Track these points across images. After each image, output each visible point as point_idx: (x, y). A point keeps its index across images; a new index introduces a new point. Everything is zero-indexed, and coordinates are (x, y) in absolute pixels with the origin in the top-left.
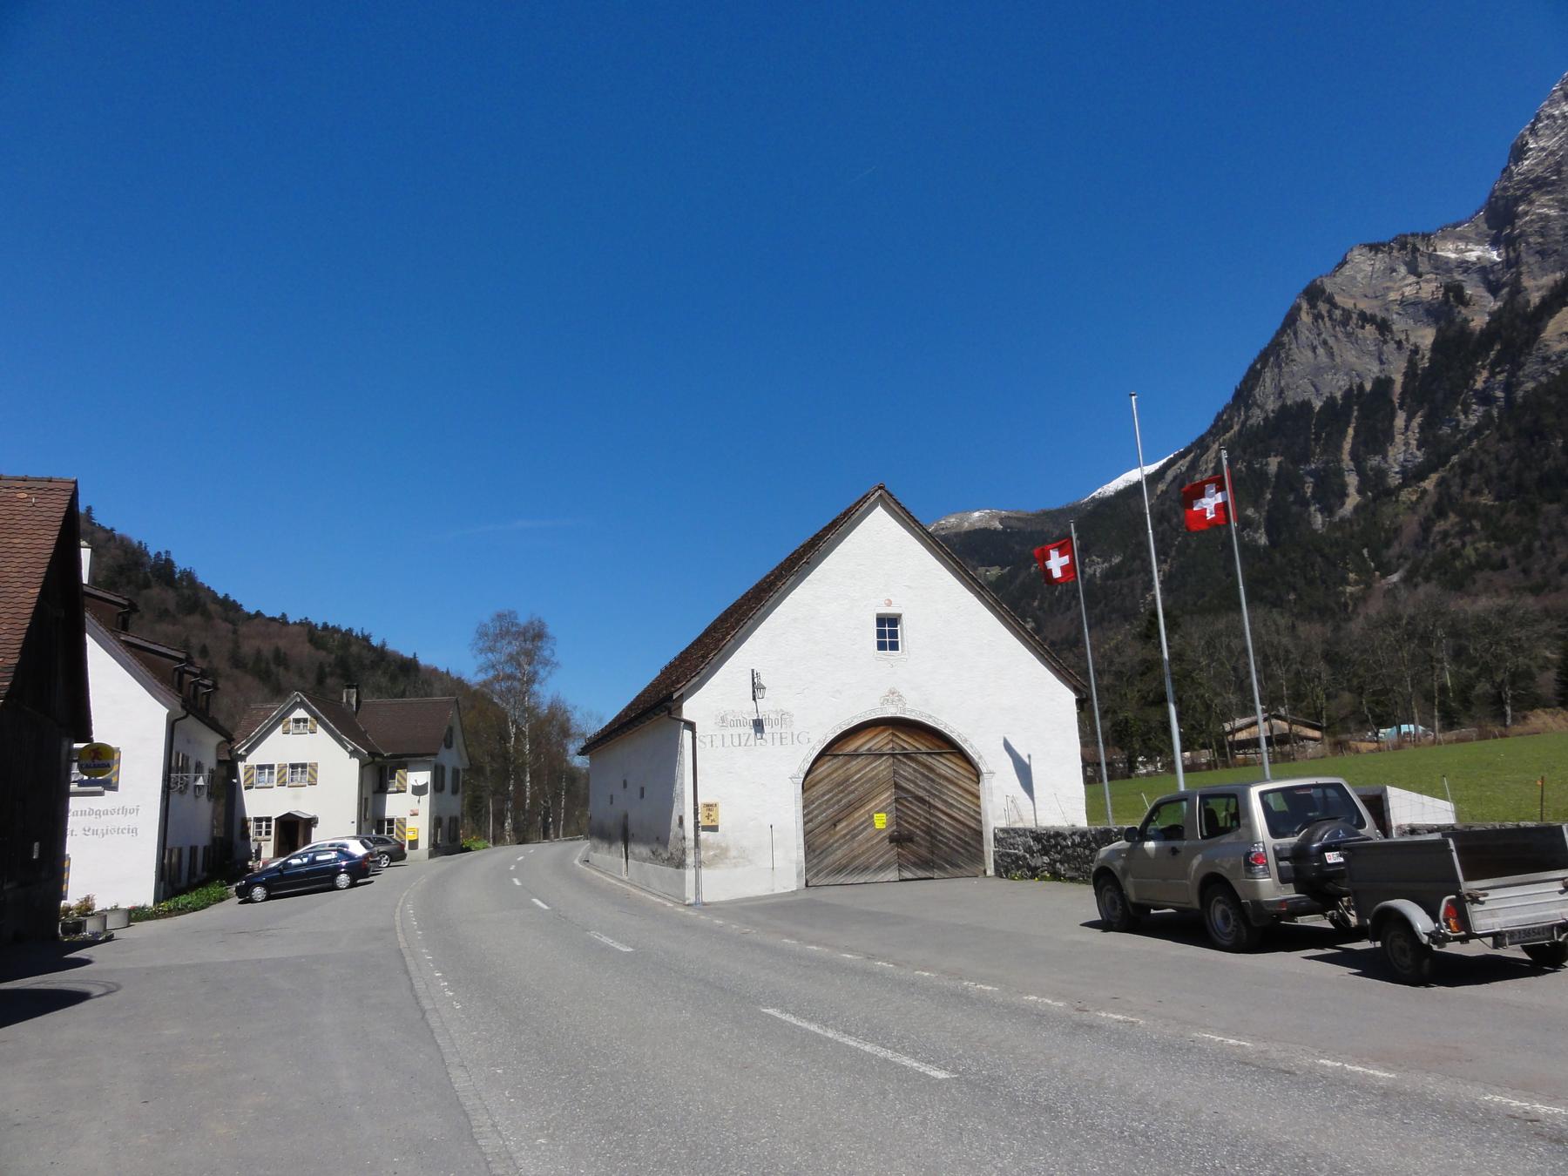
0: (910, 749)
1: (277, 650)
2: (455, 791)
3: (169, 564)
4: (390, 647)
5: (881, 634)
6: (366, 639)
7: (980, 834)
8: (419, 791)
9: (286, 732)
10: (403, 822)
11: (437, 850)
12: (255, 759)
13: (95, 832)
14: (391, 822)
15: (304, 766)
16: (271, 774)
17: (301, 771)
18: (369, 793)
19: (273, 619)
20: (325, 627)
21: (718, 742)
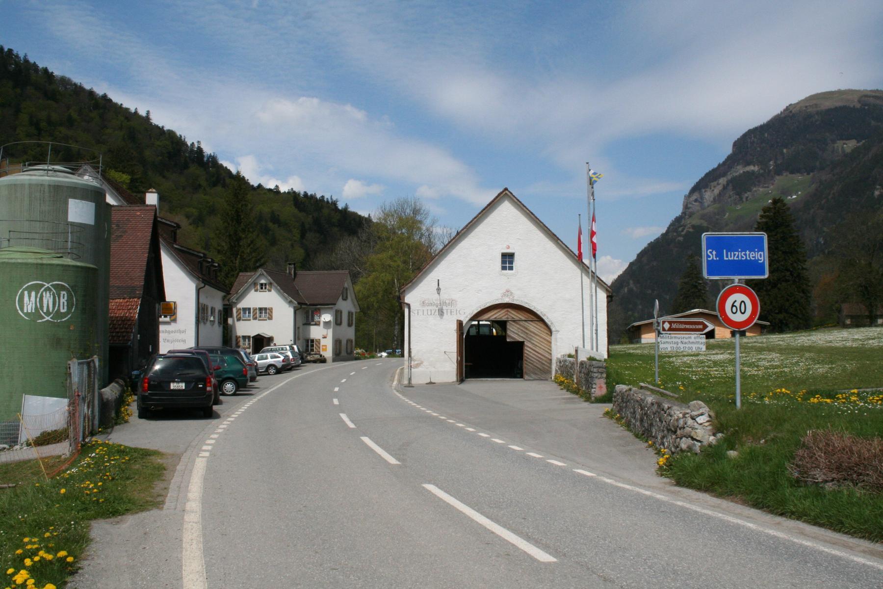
0: (516, 318)
1: (273, 213)
2: (350, 325)
3: (200, 150)
4: (352, 209)
5: (503, 262)
6: (334, 204)
7: (551, 360)
8: (327, 324)
9: (256, 291)
10: (319, 341)
11: (334, 360)
12: (241, 305)
13: (168, 341)
14: (312, 341)
15: (266, 309)
16: (249, 313)
17: (265, 313)
18: (300, 324)
19: (270, 190)
20: (306, 194)
21: (421, 313)
